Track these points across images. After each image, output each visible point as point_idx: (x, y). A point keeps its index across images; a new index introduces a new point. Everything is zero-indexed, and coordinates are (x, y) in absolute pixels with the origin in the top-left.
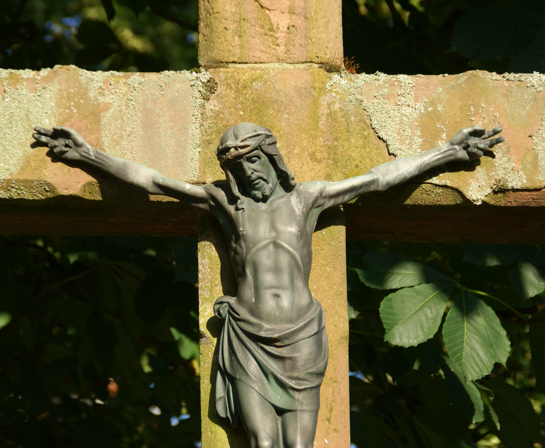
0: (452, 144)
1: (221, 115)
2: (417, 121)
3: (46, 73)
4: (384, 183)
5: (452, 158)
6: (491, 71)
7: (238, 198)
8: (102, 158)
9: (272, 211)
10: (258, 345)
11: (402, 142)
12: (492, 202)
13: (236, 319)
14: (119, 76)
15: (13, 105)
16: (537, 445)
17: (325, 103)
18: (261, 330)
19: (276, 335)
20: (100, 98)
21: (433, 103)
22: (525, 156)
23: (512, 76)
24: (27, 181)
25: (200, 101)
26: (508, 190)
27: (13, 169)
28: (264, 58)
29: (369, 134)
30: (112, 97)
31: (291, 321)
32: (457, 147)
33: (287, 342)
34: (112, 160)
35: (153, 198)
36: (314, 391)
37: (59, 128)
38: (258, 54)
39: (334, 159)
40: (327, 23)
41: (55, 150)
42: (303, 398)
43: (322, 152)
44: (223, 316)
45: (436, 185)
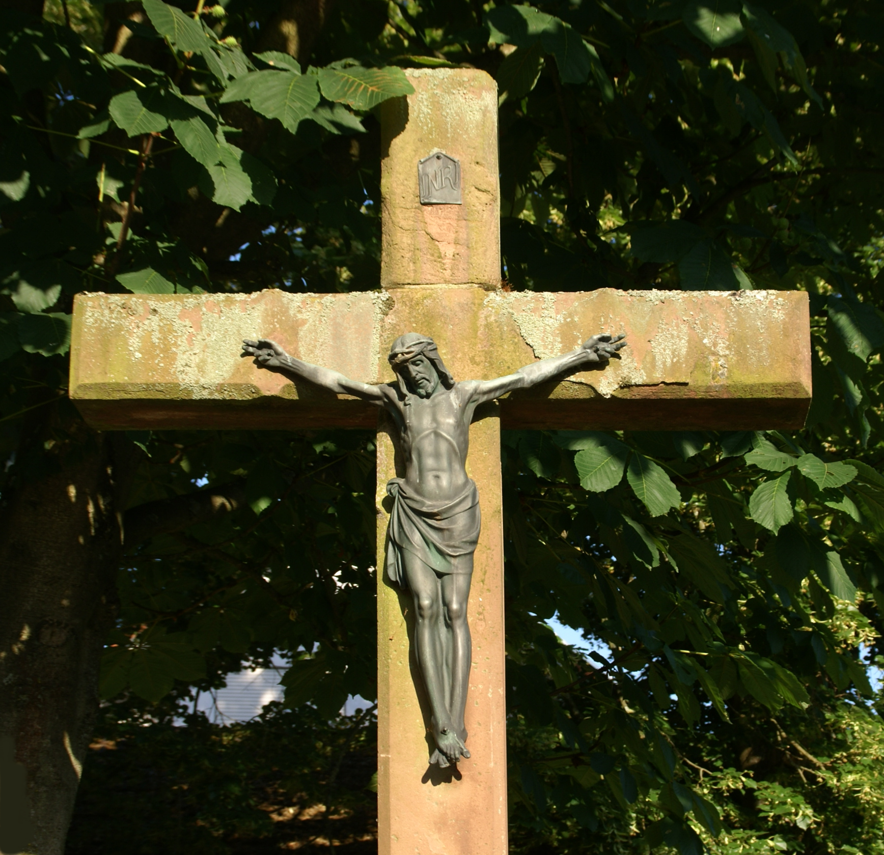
0: (585, 348)
1: (398, 327)
2: (558, 330)
3: (256, 296)
4: (529, 381)
5: (585, 359)
6: (618, 288)
7: (406, 396)
8: (297, 364)
9: (434, 406)
10: (421, 519)
11: (545, 347)
12: (620, 396)
13: (404, 498)
14: (315, 297)
15: (227, 322)
17: (483, 316)
18: (423, 506)
19: (436, 510)
20: (298, 315)
21: (570, 315)
22: (645, 358)
23: (635, 293)
24: (236, 384)
25: (380, 316)
26: (632, 386)
27: (226, 375)
28: (433, 279)
29: (518, 340)
30: (308, 314)
31: (449, 498)
32: (588, 350)
33: (445, 516)
34: (305, 366)
35: (340, 397)
36: (468, 557)
37: (263, 340)
38: (429, 277)
39: (489, 362)
40: (486, 251)
41: (260, 359)
42: (458, 563)
43: (480, 356)
44: (394, 495)
45: (574, 382)
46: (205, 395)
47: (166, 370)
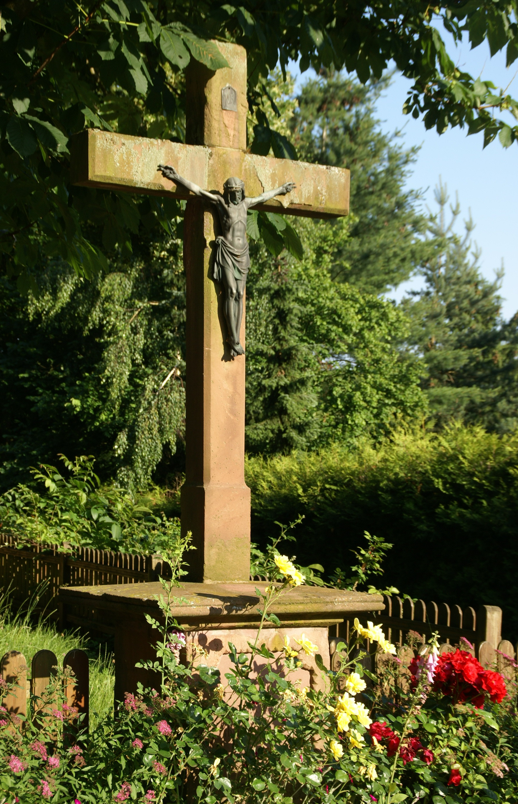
16: (2, 166)
46: (142, 186)
47: (129, 173)
